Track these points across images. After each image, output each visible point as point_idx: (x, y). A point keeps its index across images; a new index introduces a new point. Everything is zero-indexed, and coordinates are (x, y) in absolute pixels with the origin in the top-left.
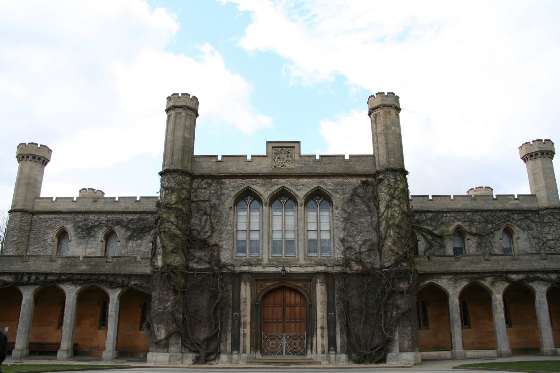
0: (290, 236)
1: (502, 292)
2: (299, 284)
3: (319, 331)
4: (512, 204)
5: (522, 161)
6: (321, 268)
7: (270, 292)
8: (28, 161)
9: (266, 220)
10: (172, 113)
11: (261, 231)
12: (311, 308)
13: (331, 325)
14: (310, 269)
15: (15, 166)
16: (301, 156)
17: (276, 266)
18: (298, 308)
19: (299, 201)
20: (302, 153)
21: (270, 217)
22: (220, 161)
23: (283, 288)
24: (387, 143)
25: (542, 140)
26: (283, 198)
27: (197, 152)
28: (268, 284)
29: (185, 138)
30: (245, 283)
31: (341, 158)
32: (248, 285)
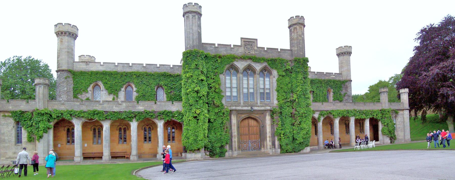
0: (251, 91)
2: (257, 116)
3: (268, 139)
5: (55, 35)
6: (269, 108)
10: (59, 73)
12: (264, 127)
13: (273, 136)
14: (263, 108)
15: (55, 39)
16: (258, 47)
19: (257, 72)
20: (259, 46)
27: (203, 41)
28: (243, 116)
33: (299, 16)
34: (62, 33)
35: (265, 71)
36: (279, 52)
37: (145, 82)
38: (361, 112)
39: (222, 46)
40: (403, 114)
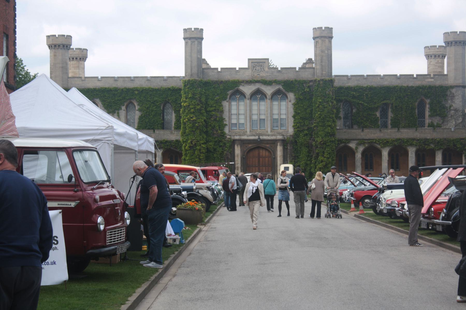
1: (388, 151)
2: (268, 146)
4: (428, 82)
6: (279, 137)
7: (251, 150)
8: (59, 49)
9: (248, 108)
11: (245, 114)
14: (273, 138)
16: (270, 68)
17: (254, 136)
18: (267, 159)
21: (251, 106)
22: (219, 72)
23: (258, 148)
24: (322, 62)
25: (436, 46)
26: (258, 94)
28: (250, 146)
29: (198, 58)
30: (237, 145)
31: (293, 70)
32: (239, 146)
33: (64, 36)
34: (55, 46)
35: (279, 95)
36: (297, 71)
37: (149, 99)
38: (426, 141)
39: (226, 70)
40: (62, 177)
